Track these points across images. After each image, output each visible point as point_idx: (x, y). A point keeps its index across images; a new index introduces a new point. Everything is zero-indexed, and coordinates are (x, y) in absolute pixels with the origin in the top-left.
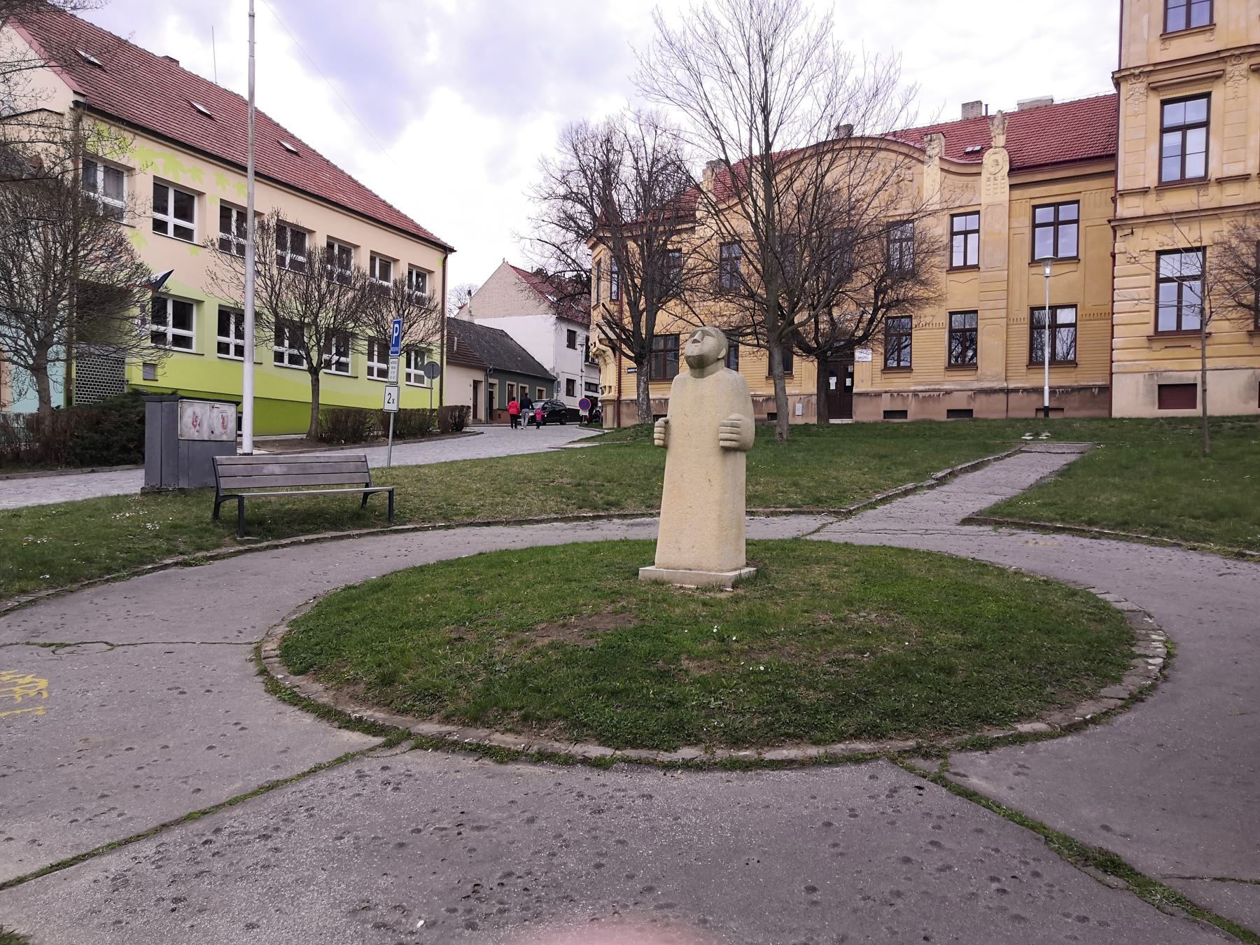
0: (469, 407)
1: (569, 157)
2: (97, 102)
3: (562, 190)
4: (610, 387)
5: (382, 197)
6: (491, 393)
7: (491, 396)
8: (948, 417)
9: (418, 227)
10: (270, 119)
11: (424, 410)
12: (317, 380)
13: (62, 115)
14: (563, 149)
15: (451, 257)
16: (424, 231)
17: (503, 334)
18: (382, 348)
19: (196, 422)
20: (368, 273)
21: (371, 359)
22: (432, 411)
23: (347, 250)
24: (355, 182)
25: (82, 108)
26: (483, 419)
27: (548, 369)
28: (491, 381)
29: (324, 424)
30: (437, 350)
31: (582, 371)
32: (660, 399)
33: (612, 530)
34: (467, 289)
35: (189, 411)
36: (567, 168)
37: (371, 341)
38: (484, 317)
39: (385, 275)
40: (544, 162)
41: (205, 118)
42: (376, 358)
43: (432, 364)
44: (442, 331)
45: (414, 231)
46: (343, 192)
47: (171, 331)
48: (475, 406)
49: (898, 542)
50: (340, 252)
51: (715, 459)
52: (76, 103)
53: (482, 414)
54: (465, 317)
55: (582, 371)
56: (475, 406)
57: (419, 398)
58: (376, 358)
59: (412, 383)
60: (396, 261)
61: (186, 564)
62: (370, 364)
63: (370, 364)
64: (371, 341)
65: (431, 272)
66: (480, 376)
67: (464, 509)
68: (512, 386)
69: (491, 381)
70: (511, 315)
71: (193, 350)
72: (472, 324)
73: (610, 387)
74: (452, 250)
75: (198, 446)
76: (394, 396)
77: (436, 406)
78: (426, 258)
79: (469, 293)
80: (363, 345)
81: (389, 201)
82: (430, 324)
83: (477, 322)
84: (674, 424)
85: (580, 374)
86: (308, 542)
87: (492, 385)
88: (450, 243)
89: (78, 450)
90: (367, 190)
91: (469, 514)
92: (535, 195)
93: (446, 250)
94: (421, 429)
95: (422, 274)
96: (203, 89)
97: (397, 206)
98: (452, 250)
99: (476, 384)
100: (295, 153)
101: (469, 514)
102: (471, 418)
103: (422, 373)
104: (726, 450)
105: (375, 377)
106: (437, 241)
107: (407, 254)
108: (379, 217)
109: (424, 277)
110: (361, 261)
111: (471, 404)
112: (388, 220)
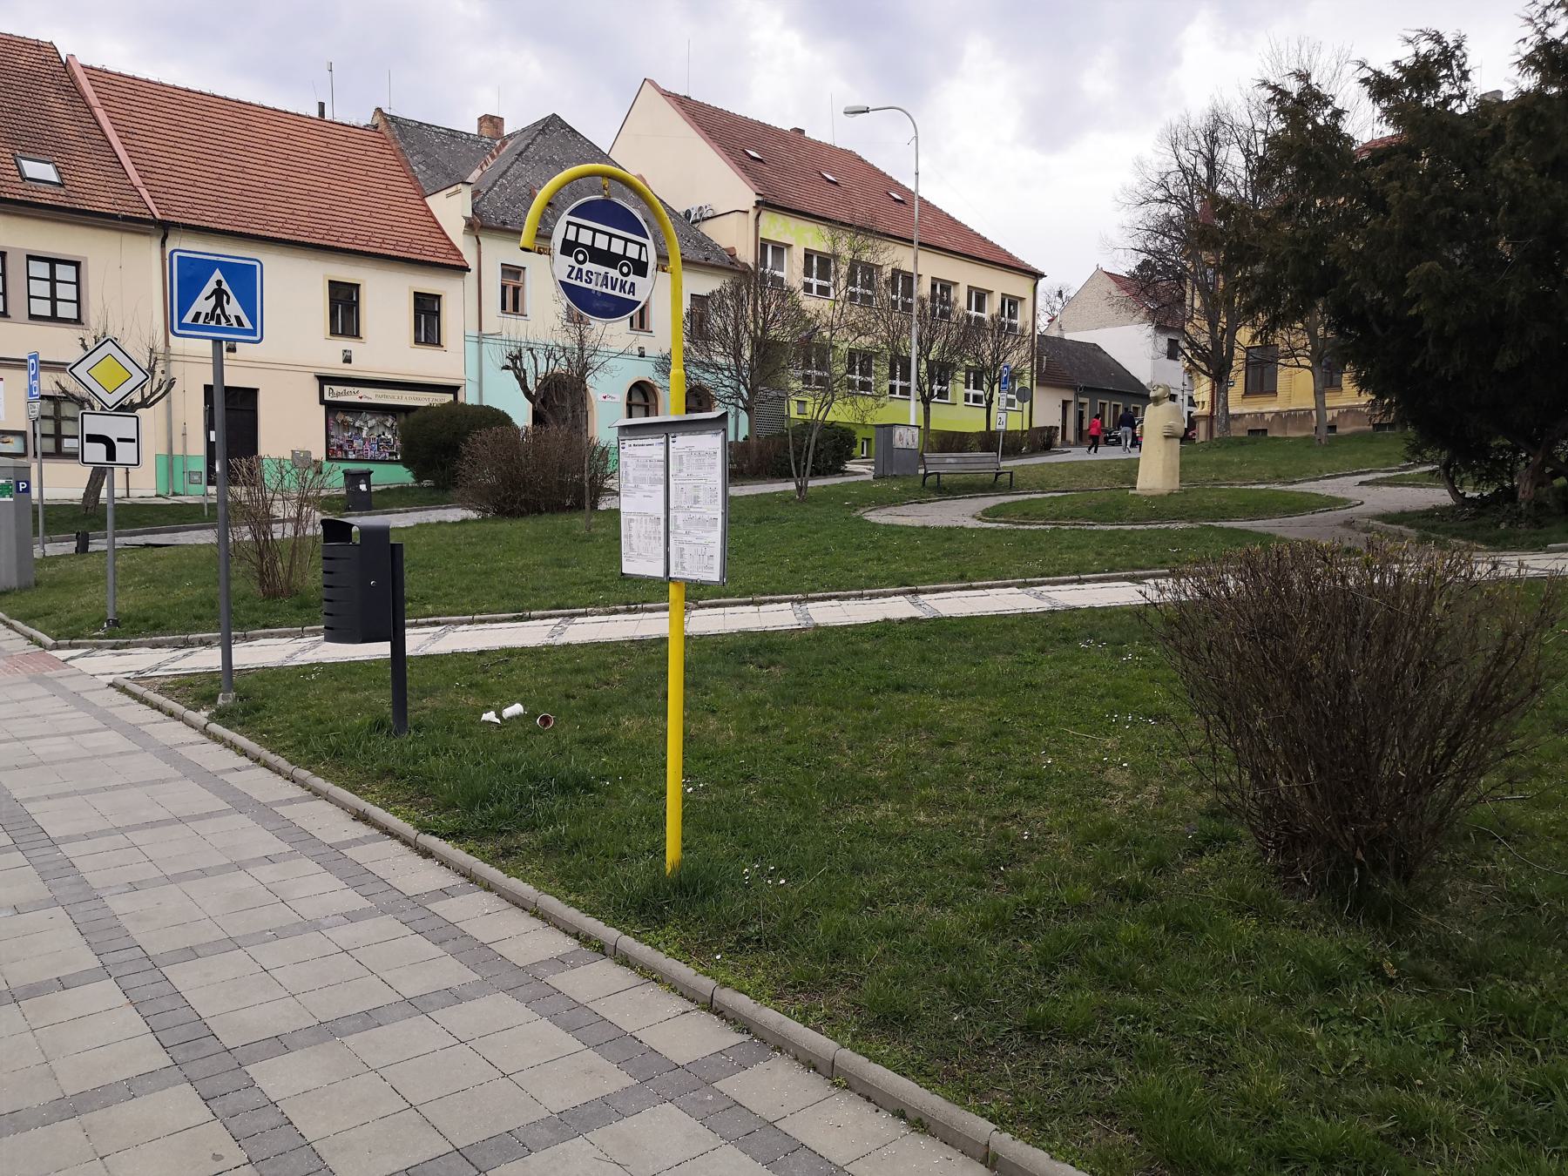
0: (1057, 428)
1: (1169, 157)
2: (771, 199)
3: (1159, 194)
4: (1203, 402)
5: (977, 230)
6: (1081, 414)
7: (1081, 416)
8: (688, 410)
9: (1010, 256)
10: (878, 170)
11: (1016, 431)
12: (929, 408)
13: (747, 212)
14: (1162, 150)
15: (1041, 282)
16: (1016, 260)
17: (1095, 348)
18: (977, 377)
19: (901, 439)
20: (966, 307)
21: (967, 387)
22: (1023, 432)
23: (947, 286)
24: (952, 219)
25: (763, 205)
26: (1072, 440)
27: (1145, 384)
28: (1082, 400)
29: (934, 445)
30: (1027, 376)
31: (1184, 384)
32: (1256, 414)
33: (1107, 453)
34: (1057, 289)
35: (898, 432)
36: (1164, 169)
37: (968, 370)
38: (1075, 330)
39: (980, 308)
40: (1140, 164)
41: (833, 186)
42: (971, 385)
43: (1023, 389)
44: (1032, 360)
45: (1007, 261)
46: (942, 233)
47: (898, 383)
48: (1064, 427)
49: (1313, 491)
50: (943, 288)
51: (1162, 442)
52: (757, 202)
53: (1071, 436)
54: (1055, 333)
55: (1184, 384)
56: (1064, 427)
57: (1010, 420)
58: (971, 385)
59: (897, 395)
60: (990, 292)
61: (919, 503)
62: (967, 391)
63: (967, 391)
64: (968, 370)
65: (1022, 299)
66: (1069, 396)
67: (1052, 484)
68: (1104, 404)
69: (1082, 400)
70: (1105, 327)
71: (948, 401)
72: (1061, 339)
73: (1203, 402)
74: (1042, 276)
75: (901, 451)
76: (1003, 419)
77: (1026, 427)
78: (1017, 286)
79: (1060, 294)
80: (961, 376)
81: (983, 234)
82: (1023, 353)
83: (1067, 336)
84: (1145, 427)
85: (1182, 387)
86: (970, 497)
87: (1082, 405)
88: (1041, 269)
89: (779, 466)
90: (963, 225)
91: (1055, 487)
92: (1129, 201)
93: (1037, 276)
94: (1013, 448)
95: (1011, 302)
96: (825, 154)
97: (990, 238)
98: (1042, 276)
99: (1065, 404)
100: (902, 202)
101: (1055, 487)
102: (1059, 437)
103: (1014, 397)
104: (1167, 437)
105: (971, 403)
106: (1028, 269)
107: (1000, 284)
108: (975, 253)
109: (1015, 305)
110: (960, 297)
111: (1059, 424)
112: (984, 256)
